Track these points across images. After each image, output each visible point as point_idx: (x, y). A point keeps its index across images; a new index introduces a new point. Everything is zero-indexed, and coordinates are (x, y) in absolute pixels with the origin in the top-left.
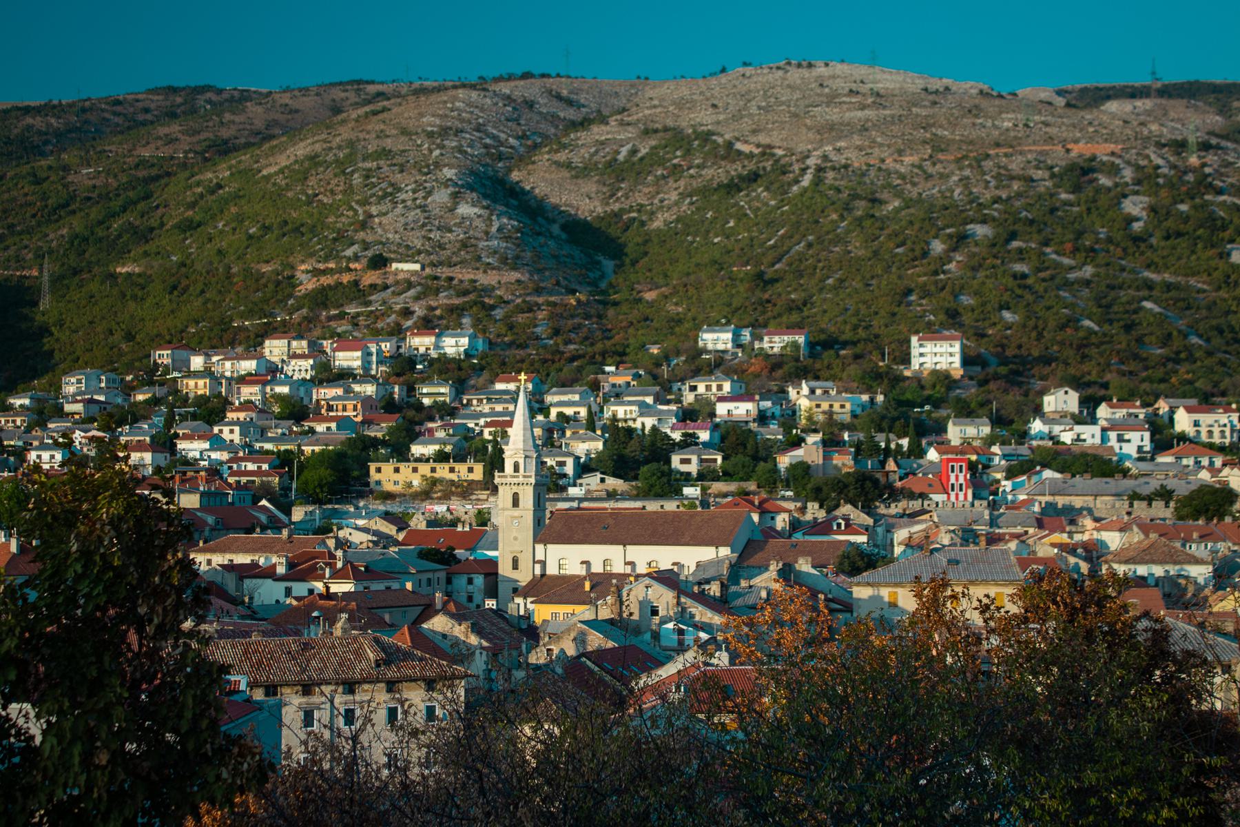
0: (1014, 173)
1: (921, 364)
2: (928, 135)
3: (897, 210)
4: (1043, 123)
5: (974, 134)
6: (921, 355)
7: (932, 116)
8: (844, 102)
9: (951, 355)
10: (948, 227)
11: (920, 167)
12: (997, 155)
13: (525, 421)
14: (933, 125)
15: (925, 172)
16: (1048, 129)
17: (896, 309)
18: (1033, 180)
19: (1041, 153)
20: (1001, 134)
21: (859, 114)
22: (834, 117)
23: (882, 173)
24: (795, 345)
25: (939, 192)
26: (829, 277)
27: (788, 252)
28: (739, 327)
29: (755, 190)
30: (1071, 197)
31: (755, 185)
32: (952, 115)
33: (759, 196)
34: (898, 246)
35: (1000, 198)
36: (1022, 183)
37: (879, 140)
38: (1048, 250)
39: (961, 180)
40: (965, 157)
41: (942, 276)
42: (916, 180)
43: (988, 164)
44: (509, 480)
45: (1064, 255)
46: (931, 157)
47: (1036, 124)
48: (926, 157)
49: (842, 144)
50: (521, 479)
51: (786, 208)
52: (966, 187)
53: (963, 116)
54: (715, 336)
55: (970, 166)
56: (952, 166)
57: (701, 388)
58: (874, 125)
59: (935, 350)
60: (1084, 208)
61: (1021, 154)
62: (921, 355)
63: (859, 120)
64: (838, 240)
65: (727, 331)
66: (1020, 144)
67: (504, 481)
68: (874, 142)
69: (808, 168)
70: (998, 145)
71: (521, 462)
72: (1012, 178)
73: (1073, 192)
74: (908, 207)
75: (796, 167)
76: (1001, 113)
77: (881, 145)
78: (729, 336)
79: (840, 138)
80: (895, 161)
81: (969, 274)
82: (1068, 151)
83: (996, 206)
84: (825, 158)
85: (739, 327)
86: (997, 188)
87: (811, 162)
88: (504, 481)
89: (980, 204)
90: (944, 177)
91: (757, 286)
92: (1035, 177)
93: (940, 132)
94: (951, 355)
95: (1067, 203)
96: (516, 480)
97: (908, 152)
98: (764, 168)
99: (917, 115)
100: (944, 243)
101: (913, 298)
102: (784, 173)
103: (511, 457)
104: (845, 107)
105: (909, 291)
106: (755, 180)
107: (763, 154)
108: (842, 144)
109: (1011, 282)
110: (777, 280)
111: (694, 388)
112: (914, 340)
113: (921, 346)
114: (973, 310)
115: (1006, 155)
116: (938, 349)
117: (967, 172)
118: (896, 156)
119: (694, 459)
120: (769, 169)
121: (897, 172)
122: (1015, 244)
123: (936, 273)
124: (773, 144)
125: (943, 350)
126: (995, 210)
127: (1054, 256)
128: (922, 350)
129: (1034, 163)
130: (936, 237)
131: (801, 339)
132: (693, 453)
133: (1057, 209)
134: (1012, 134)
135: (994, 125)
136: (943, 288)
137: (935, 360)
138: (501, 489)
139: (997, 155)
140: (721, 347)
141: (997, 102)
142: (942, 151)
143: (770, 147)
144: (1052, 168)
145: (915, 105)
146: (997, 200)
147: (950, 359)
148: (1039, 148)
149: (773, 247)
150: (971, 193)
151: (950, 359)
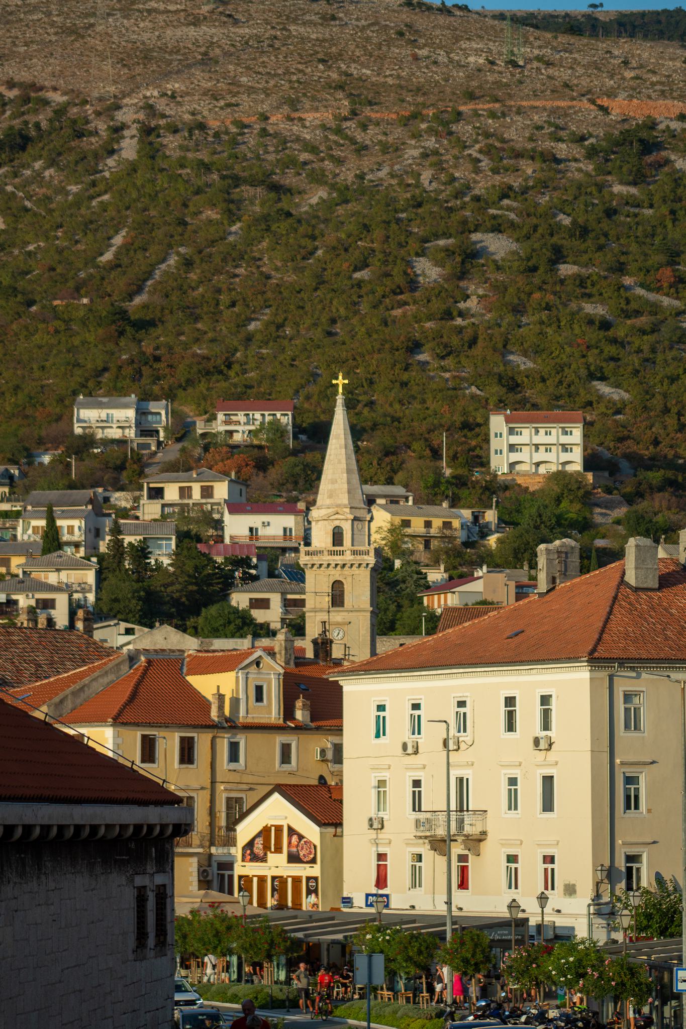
0: (518, 146)
1: (512, 465)
2: (334, 76)
3: (328, 205)
4: (539, 59)
5: (420, 76)
6: (512, 448)
7: (332, 41)
8: (155, 10)
9: (565, 448)
10: (437, 236)
11: (339, 131)
12: (476, 113)
13: (348, 458)
14: (340, 56)
15: (353, 141)
16: (550, 71)
17: (405, 377)
18: (558, 161)
19: (554, 111)
20: (469, 77)
21: (192, 32)
22: (145, 36)
23: (270, 142)
24: (276, 428)
25: (392, 175)
26: (251, 320)
27: (149, 274)
28: (146, 397)
29: (27, 166)
30: (633, 190)
31: (25, 157)
32: (368, 39)
33: (38, 175)
34: (356, 269)
35: (510, 188)
36: (538, 165)
37: (244, 79)
38: (628, 281)
39: (425, 156)
40: (415, 116)
41: (459, 321)
42: (337, 153)
43: (464, 129)
44: (326, 558)
45: (658, 290)
46: (354, 113)
47: (528, 61)
48: (345, 112)
49: (175, 85)
50: (348, 557)
51: (106, 197)
52: (439, 166)
53: (389, 42)
54: (104, 413)
55: (430, 131)
56: (398, 132)
57: (172, 493)
58: (227, 54)
59: (537, 440)
60: (664, 210)
61: (518, 113)
62: (512, 448)
63: (196, 43)
64: (237, 256)
65: (126, 406)
66: (510, 96)
67: (316, 559)
68: (235, 83)
69: (123, 126)
70: (471, 96)
71: (347, 527)
72: (518, 155)
73: (634, 184)
74: (346, 201)
75: (102, 126)
76: (457, 39)
77: (251, 90)
78: (131, 413)
79: (167, 75)
80: (290, 119)
81: (509, 318)
82: (605, 110)
83: (506, 202)
84: (150, 108)
85: (146, 397)
86: (496, 171)
87: (125, 115)
88: (316, 559)
89: (477, 199)
90: (391, 150)
91: (121, 333)
92: (561, 155)
93: (354, 70)
94: (565, 448)
95: (628, 201)
96: (338, 559)
97: (307, 104)
98: (37, 126)
99: (303, 39)
100: (438, 263)
101: (423, 357)
102: (80, 135)
103: (327, 519)
104: (161, 18)
105: (415, 347)
106: (23, 148)
107: (26, 100)
108: (175, 85)
109: (593, 335)
110: (152, 324)
111: (157, 493)
112: (497, 423)
113: (511, 431)
114: (543, 380)
115: (493, 115)
116: (541, 438)
117: (431, 143)
118: (286, 109)
119: (275, 599)
120: (44, 125)
121: (298, 139)
122: (566, 270)
123: (448, 315)
124: (40, 82)
125: (551, 439)
126: (509, 209)
127: (640, 291)
128: (514, 440)
129: (548, 130)
130: (421, 253)
131: (285, 419)
132: (272, 590)
133: (615, 212)
134: (490, 78)
135: (451, 61)
136: (473, 342)
137: (537, 457)
138: (309, 575)
139: (476, 113)
140: (114, 433)
141: (442, 20)
142: (370, 103)
143: (34, 87)
144: (583, 138)
145: (295, 21)
146: (506, 192)
147: (565, 457)
148: (549, 104)
149: (115, 265)
150: (453, 179)
151: (565, 457)
